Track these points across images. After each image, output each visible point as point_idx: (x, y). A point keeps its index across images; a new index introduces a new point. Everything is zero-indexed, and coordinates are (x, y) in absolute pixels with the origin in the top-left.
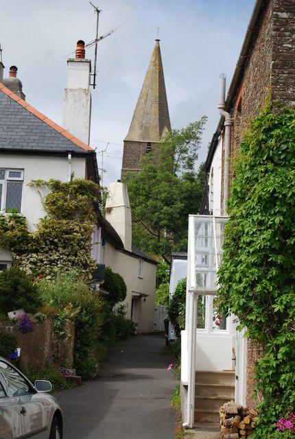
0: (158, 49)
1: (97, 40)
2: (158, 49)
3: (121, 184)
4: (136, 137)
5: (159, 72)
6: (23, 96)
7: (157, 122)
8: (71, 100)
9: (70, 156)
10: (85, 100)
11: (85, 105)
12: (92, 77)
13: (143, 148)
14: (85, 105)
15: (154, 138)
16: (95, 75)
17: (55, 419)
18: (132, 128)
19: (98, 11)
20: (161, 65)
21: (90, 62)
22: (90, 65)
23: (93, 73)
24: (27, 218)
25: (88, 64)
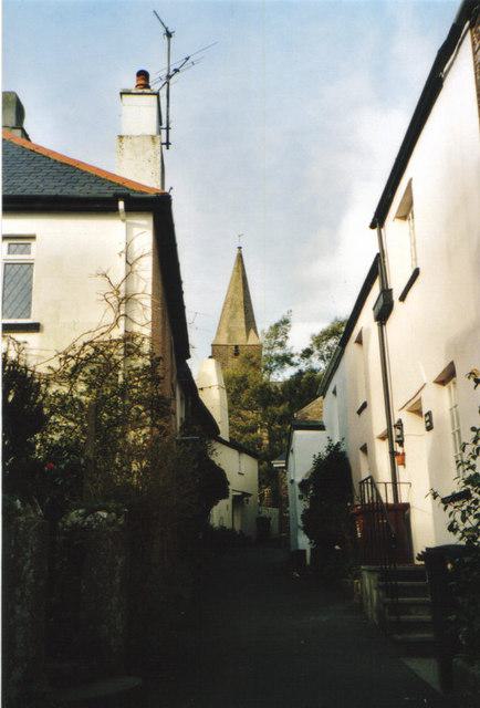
0: (240, 258)
1: (169, 77)
2: (240, 258)
3: (212, 361)
4: (223, 341)
5: (245, 302)
6: (25, 136)
7: (243, 325)
8: (127, 153)
9: (121, 205)
10: (151, 152)
11: (152, 160)
12: (164, 132)
13: (231, 352)
14: (152, 160)
15: (240, 339)
16: (168, 128)
17: (381, 300)
18: (218, 333)
19: (169, 35)
20: (244, 270)
21: (157, 94)
22: (158, 98)
23: (164, 126)
24: (64, 345)
25: (156, 97)
